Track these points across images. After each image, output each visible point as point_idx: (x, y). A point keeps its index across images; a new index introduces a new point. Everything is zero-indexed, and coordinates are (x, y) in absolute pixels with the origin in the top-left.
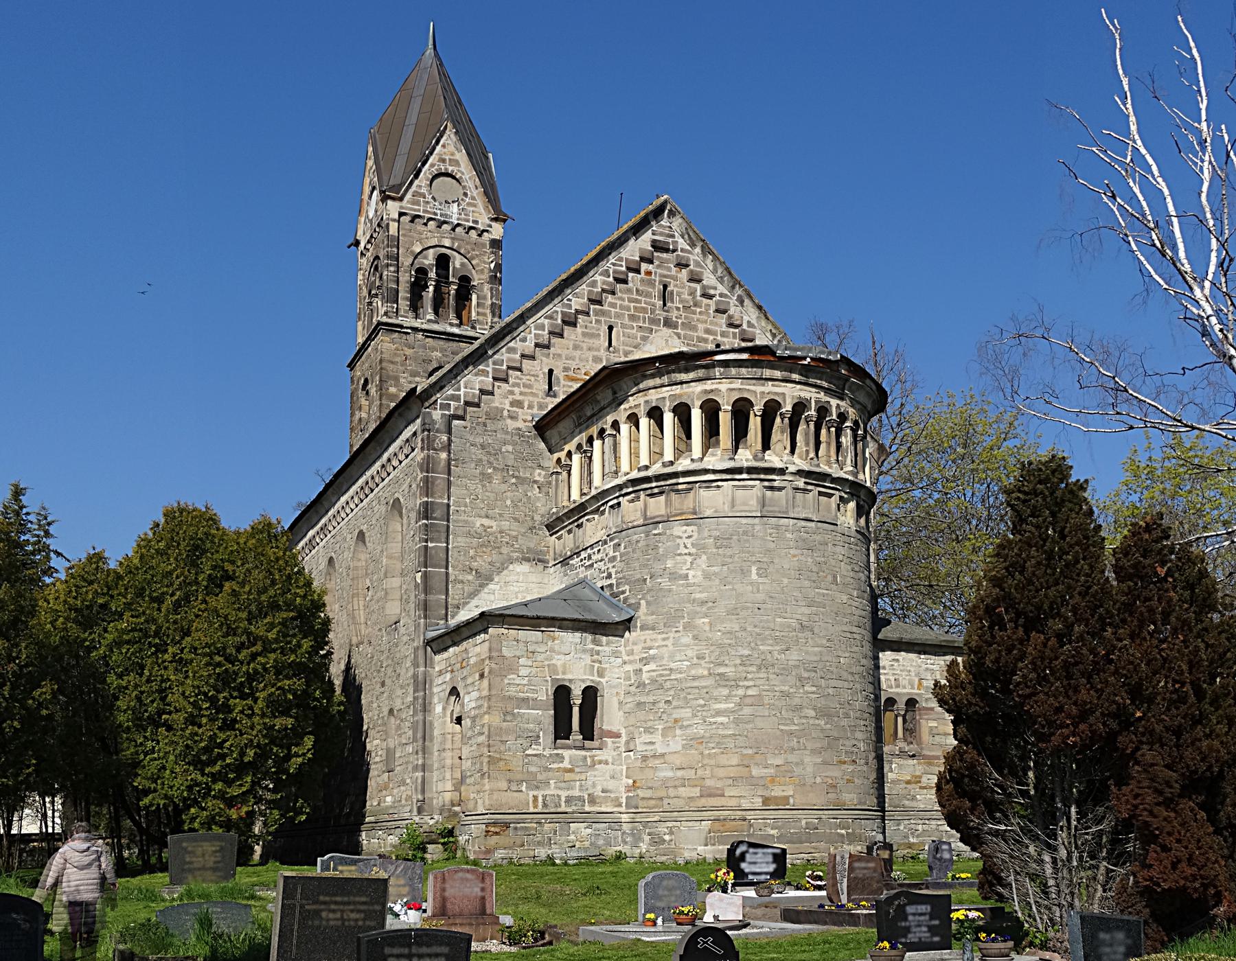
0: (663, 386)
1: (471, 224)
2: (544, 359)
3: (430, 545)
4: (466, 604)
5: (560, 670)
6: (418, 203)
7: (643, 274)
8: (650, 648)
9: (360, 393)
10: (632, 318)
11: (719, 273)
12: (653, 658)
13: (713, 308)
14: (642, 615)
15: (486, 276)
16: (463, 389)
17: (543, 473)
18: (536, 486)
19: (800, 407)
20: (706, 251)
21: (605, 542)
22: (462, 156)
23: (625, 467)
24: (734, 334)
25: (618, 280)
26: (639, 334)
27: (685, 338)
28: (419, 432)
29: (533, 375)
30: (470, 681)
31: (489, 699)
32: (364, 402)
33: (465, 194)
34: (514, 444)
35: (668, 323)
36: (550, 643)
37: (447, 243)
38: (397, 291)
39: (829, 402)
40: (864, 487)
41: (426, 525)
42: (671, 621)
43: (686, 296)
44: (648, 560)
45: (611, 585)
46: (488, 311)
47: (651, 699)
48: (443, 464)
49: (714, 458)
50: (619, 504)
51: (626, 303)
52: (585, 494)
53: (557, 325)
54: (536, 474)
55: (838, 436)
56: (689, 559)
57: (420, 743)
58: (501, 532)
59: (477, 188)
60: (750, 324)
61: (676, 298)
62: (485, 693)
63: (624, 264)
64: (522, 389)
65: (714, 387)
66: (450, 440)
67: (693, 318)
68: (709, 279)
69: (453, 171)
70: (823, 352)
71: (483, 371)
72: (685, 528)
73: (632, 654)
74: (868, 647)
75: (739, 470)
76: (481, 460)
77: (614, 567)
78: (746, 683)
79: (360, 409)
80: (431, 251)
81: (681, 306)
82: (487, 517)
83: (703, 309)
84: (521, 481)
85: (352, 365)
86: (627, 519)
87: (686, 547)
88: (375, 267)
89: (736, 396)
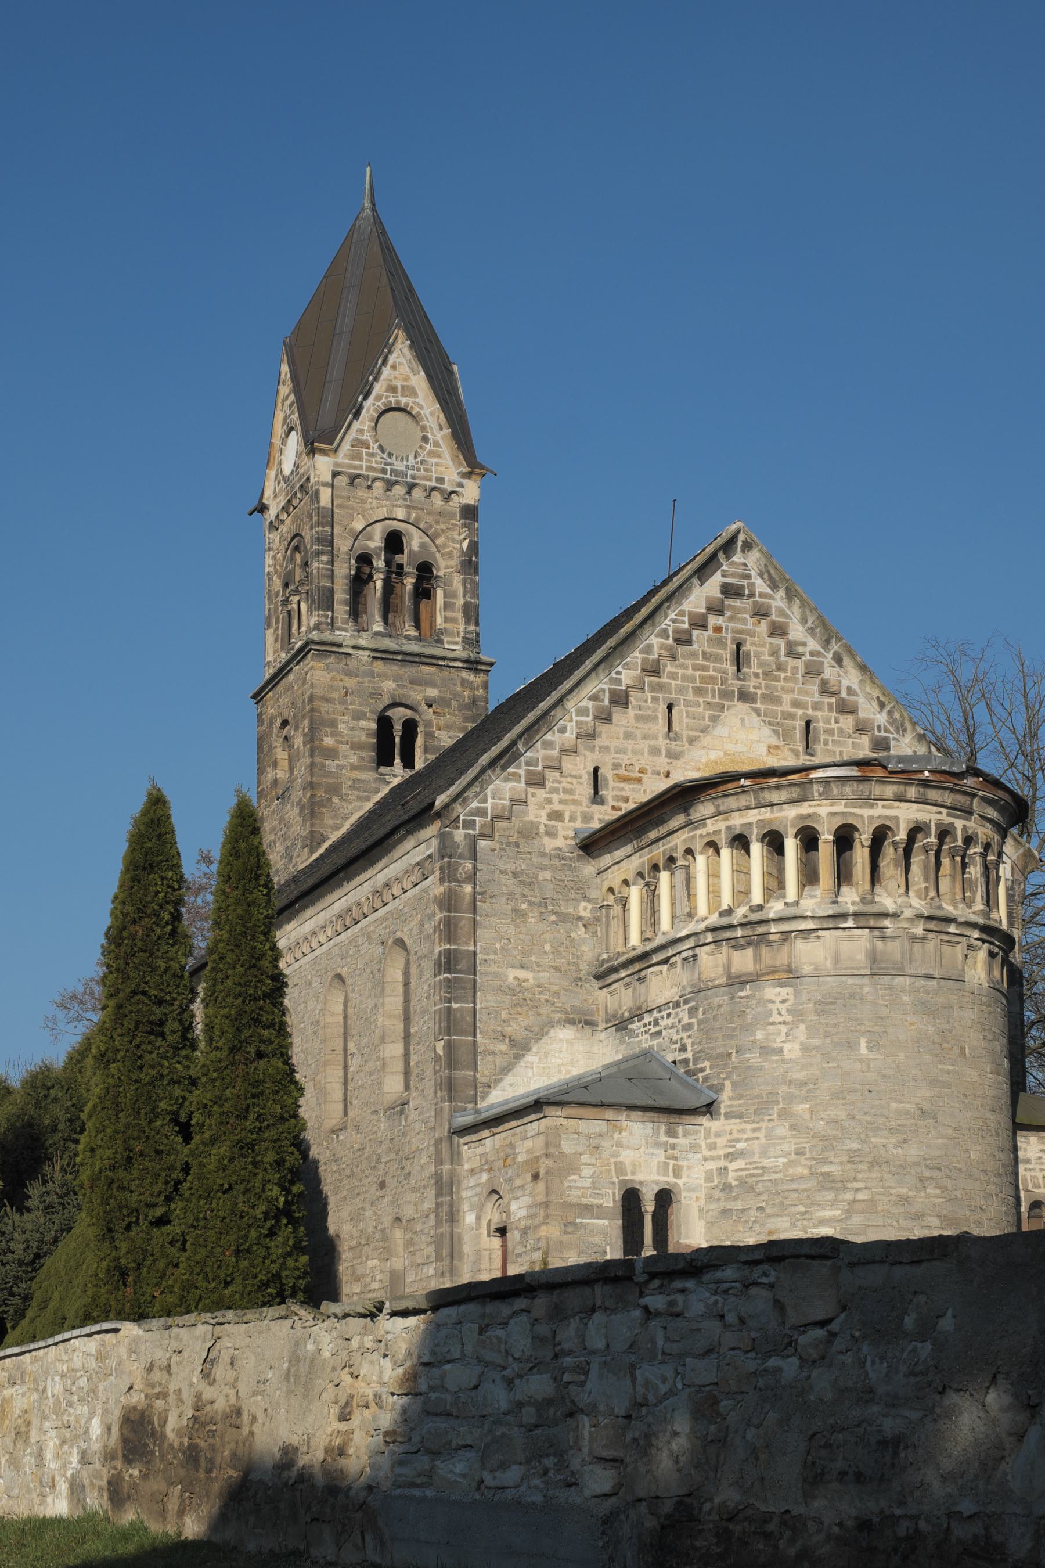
0: (749, 808)
1: (434, 484)
2: (588, 753)
3: (455, 1006)
4: (498, 1081)
5: (629, 1169)
6: (358, 457)
7: (710, 632)
8: (738, 1141)
9: (277, 742)
10: (699, 691)
11: (809, 624)
12: (741, 1154)
13: (801, 670)
14: (726, 1099)
15: (455, 562)
16: (490, 800)
17: (590, 906)
18: (580, 924)
19: (916, 831)
20: (790, 595)
21: (677, 1005)
22: (419, 381)
23: (702, 909)
24: (830, 705)
25: (679, 641)
26: (707, 714)
27: (766, 715)
28: (436, 856)
29: (575, 777)
30: (518, 1182)
31: (547, 1206)
32: (282, 755)
33: (425, 439)
34: (553, 868)
35: (745, 696)
36: (616, 1136)
37: (400, 513)
38: (332, 592)
39: (952, 824)
40: (1000, 930)
41: (449, 980)
42: (763, 1106)
43: (767, 658)
44: (734, 1029)
45: (686, 1061)
46: (460, 615)
47: (739, 1205)
48: (468, 899)
49: (814, 901)
50: (695, 956)
51: (690, 672)
52: (648, 939)
53: (604, 708)
54: (581, 908)
55: (964, 865)
56: (784, 1029)
57: (447, 1262)
58: (539, 986)
59: (441, 429)
60: (850, 691)
61: (754, 661)
62: (541, 1198)
63: (686, 619)
64: (562, 796)
65: (811, 811)
66: (475, 867)
67: (776, 687)
68: (797, 631)
69: (407, 404)
70: (944, 764)
71: (514, 774)
72: (778, 989)
73: (715, 1148)
74: (1003, 1119)
75: (844, 916)
76: (512, 893)
77: (689, 1037)
78: (856, 1185)
79: (275, 764)
80: (378, 527)
81: (760, 671)
82: (522, 967)
83: (789, 674)
84: (563, 918)
85: (258, 696)
86: (704, 977)
87: (780, 1014)
88: (295, 543)
89: (838, 822)
